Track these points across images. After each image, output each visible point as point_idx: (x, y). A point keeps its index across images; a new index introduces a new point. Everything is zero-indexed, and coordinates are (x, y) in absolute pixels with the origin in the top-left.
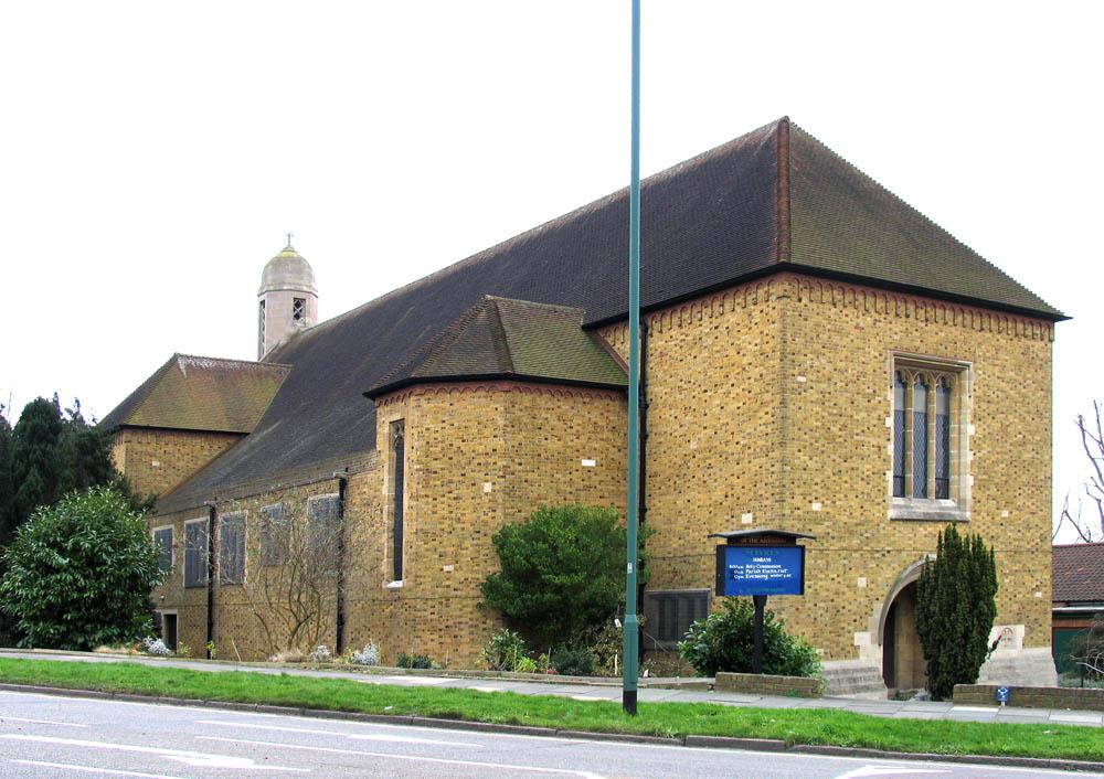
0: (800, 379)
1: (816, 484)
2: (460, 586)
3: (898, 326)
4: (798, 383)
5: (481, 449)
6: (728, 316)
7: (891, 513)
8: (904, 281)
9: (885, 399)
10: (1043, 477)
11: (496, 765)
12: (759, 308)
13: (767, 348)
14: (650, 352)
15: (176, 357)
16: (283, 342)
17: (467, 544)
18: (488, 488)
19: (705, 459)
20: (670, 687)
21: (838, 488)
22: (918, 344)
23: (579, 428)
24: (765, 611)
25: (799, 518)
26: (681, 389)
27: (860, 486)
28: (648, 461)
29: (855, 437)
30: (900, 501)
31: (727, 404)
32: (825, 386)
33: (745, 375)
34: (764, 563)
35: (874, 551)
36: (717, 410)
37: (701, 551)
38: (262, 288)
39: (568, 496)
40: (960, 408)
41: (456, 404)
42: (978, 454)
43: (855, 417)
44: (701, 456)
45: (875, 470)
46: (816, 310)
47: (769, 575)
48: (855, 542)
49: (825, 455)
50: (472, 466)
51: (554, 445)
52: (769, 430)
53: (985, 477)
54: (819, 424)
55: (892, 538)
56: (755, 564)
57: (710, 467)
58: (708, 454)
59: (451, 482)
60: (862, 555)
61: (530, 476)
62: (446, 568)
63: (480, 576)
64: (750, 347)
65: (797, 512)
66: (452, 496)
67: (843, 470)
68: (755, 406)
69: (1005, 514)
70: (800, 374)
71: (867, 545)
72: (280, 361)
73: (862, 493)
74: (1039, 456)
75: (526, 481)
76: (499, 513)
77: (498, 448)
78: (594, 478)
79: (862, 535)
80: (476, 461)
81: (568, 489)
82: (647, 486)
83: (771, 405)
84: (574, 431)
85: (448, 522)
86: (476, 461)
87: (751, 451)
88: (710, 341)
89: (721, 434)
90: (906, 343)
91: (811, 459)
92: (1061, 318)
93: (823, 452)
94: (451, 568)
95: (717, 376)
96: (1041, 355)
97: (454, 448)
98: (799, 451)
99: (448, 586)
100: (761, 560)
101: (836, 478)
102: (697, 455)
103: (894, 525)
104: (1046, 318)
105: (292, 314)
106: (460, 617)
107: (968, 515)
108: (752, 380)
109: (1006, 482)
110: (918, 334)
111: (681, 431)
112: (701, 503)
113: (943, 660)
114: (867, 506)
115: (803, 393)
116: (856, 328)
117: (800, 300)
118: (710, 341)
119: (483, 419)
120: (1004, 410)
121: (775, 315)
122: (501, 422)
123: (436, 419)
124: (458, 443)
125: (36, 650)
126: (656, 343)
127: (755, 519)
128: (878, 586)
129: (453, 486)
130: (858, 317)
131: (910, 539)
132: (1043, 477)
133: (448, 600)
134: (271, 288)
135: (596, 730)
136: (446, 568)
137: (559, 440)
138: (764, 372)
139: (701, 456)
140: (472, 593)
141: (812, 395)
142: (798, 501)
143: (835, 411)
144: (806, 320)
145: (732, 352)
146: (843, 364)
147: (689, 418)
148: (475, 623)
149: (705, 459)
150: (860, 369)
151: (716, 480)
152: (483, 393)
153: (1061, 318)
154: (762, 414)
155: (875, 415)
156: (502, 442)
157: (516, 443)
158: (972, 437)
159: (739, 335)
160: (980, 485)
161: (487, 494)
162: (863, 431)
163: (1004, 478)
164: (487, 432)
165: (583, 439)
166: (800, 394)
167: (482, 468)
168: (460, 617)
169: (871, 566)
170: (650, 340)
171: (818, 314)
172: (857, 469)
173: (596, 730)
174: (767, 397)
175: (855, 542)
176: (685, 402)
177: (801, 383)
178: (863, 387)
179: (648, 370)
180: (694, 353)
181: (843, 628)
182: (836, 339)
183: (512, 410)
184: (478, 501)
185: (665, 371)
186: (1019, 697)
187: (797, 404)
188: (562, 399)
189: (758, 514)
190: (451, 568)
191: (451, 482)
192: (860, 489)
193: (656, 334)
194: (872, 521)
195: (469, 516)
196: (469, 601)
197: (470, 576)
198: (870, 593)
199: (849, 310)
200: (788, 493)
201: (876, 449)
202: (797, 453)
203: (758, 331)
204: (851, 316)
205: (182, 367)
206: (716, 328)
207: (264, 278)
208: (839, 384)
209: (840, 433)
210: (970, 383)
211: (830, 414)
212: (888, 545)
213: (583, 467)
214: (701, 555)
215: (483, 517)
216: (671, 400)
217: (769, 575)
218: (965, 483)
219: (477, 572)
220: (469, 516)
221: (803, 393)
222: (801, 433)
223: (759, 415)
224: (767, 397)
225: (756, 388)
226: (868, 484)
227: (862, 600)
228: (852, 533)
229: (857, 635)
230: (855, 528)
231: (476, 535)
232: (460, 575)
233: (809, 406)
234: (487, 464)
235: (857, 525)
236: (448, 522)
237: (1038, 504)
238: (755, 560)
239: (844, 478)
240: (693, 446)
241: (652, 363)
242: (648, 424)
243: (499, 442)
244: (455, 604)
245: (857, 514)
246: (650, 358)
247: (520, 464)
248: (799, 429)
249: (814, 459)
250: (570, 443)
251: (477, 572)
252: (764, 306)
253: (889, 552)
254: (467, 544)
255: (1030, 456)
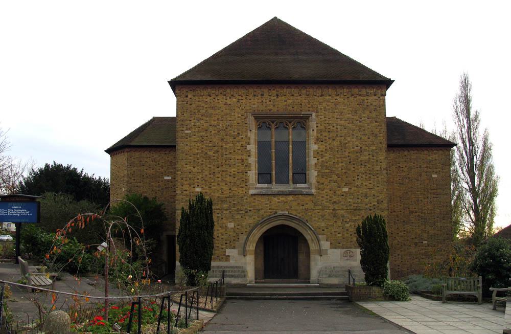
0: (187, 132)
1: (198, 179)
4: (186, 134)
7: (252, 192)
8: (222, 78)
9: (246, 137)
10: (379, 169)
11: (39, 288)
21: (212, 181)
22: (271, 107)
23: (163, 164)
25: (187, 195)
27: (229, 179)
29: (225, 156)
32: (204, 133)
34: (19, 209)
35: (238, 210)
39: (158, 192)
42: (321, 160)
43: (225, 146)
45: (240, 171)
46: (197, 100)
47: (20, 214)
48: (225, 206)
49: (204, 165)
51: (150, 172)
53: (327, 171)
54: (200, 151)
55: (254, 204)
56: (13, 209)
60: (230, 212)
61: (139, 184)
65: (185, 192)
67: (216, 172)
69: (346, 189)
70: (187, 130)
71: (234, 207)
73: (230, 182)
74: (375, 158)
75: (137, 186)
78: (171, 184)
79: (230, 202)
81: (158, 189)
84: (160, 165)
90: (262, 108)
91: (194, 168)
93: (202, 164)
96: (374, 104)
98: (186, 164)
100: (16, 207)
101: (212, 176)
103: (254, 197)
107: (313, 191)
109: (345, 173)
110: (271, 103)
114: (234, 188)
115: (189, 138)
116: (225, 105)
117: (187, 96)
120: (343, 135)
128: (242, 227)
130: (226, 100)
131: (267, 204)
132: (379, 169)
137: (153, 169)
141: (194, 138)
142: (185, 187)
143: (210, 145)
144: (191, 105)
146: (216, 122)
150: (229, 124)
155: (239, 145)
157: (132, 171)
158: (317, 153)
160: (321, 175)
162: (230, 153)
163: (344, 171)
165: (165, 168)
166: (187, 138)
169: (236, 217)
171: (199, 101)
172: (226, 171)
175: (225, 206)
177: (187, 133)
178: (231, 132)
181: (218, 247)
182: (211, 111)
183: (130, 159)
187: (185, 143)
188: (154, 153)
192: (229, 181)
194: (238, 196)
198: (237, 230)
199: (220, 97)
200: (179, 184)
201: (241, 161)
202: (185, 166)
204: (221, 99)
208: (213, 132)
209: (214, 155)
210: (313, 124)
211: (207, 146)
212: (250, 207)
213: (165, 180)
217: (20, 214)
218: (313, 174)
221: (189, 138)
222: (188, 156)
226: (234, 178)
227: (231, 233)
228: (223, 201)
229: (227, 251)
230: (225, 199)
233: (193, 144)
235: (226, 198)
237: (375, 183)
238: (13, 207)
239: (217, 176)
245: (228, 192)
247: (134, 180)
248: (187, 155)
249: (197, 167)
250: (158, 170)
253: (250, 210)
255: (367, 158)
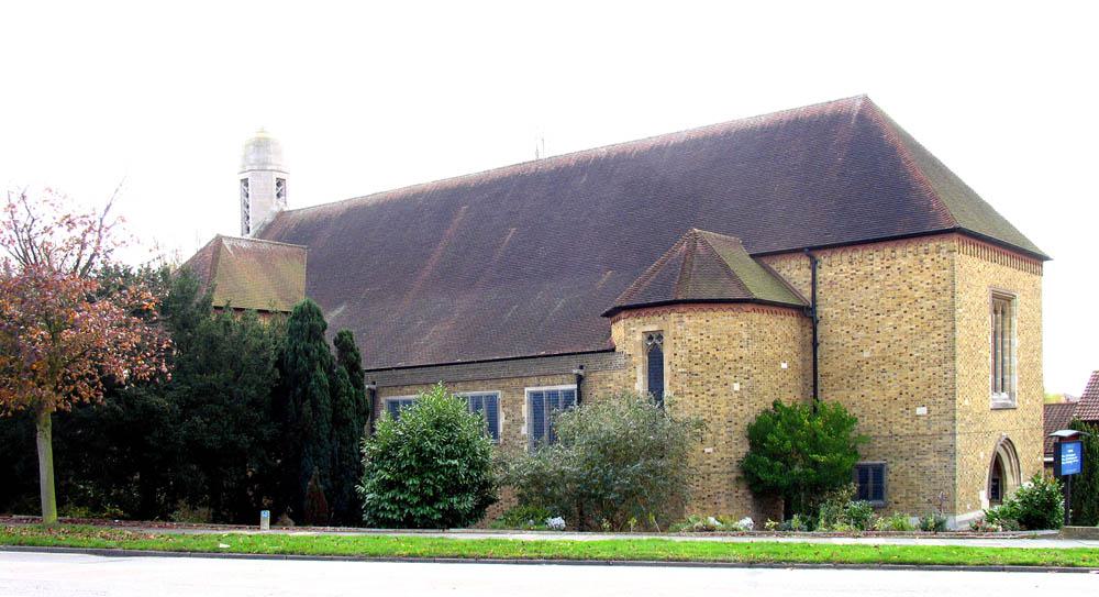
2: (717, 464)
3: (993, 268)
5: (731, 357)
6: (900, 260)
12: (929, 257)
13: (939, 288)
14: (819, 281)
15: (219, 240)
16: (269, 220)
17: (722, 431)
18: (737, 387)
19: (878, 365)
20: (1034, 538)
24: (369, 447)
26: (852, 311)
28: (819, 364)
30: (996, 396)
31: (900, 325)
33: (918, 306)
36: (890, 330)
37: (876, 433)
38: (244, 166)
40: (1010, 327)
41: (711, 321)
44: (875, 363)
50: (725, 370)
52: (942, 348)
57: (884, 371)
58: (881, 362)
59: (709, 382)
62: (707, 450)
63: (733, 456)
64: (922, 285)
66: (710, 393)
68: (928, 329)
72: (278, 238)
76: (745, 407)
77: (743, 355)
80: (727, 366)
82: (819, 384)
83: (943, 329)
85: (707, 414)
86: (727, 366)
87: (925, 362)
88: (882, 277)
89: (894, 347)
92: (1047, 259)
94: (710, 450)
95: (890, 304)
97: (711, 355)
99: (709, 464)
102: (871, 362)
104: (1032, 258)
105: (275, 193)
106: (719, 488)
107: (1016, 404)
108: (924, 310)
111: (852, 343)
112: (875, 398)
113: (1085, 509)
118: (882, 277)
119: (732, 333)
121: (946, 263)
122: (745, 336)
123: (696, 332)
124: (713, 352)
125: (452, 530)
126: (825, 273)
127: (929, 411)
129: (711, 386)
133: (709, 475)
134: (255, 167)
135: (1069, 565)
136: (707, 450)
138: (936, 304)
139: (875, 363)
140: (726, 470)
145: (905, 287)
147: (862, 333)
148: (730, 492)
149: (878, 365)
151: (890, 382)
152: (730, 313)
153: (1047, 259)
154: (935, 335)
156: (746, 352)
159: (910, 275)
161: (736, 392)
164: (735, 343)
167: (732, 371)
168: (719, 488)
170: (818, 270)
173: (1069, 565)
174: (938, 323)
176: (857, 321)
179: (817, 294)
180: (865, 284)
184: (730, 397)
185: (835, 296)
186: (977, 529)
189: (933, 408)
190: (710, 450)
191: (709, 382)
193: (824, 267)
195: (724, 409)
196: (725, 476)
197: (725, 456)
203: (929, 274)
205: (229, 248)
206: (888, 267)
207: (245, 157)
214: (876, 437)
215: (734, 410)
216: (843, 319)
219: (730, 453)
220: (724, 409)
223: (931, 335)
224: (938, 323)
225: (928, 315)
231: (728, 424)
232: (717, 456)
234: (736, 369)
236: (707, 414)
240: (866, 354)
241: (821, 289)
242: (818, 336)
243: (744, 352)
244: (714, 478)
246: (819, 285)
251: (730, 453)
252: (935, 256)
254: (722, 431)
